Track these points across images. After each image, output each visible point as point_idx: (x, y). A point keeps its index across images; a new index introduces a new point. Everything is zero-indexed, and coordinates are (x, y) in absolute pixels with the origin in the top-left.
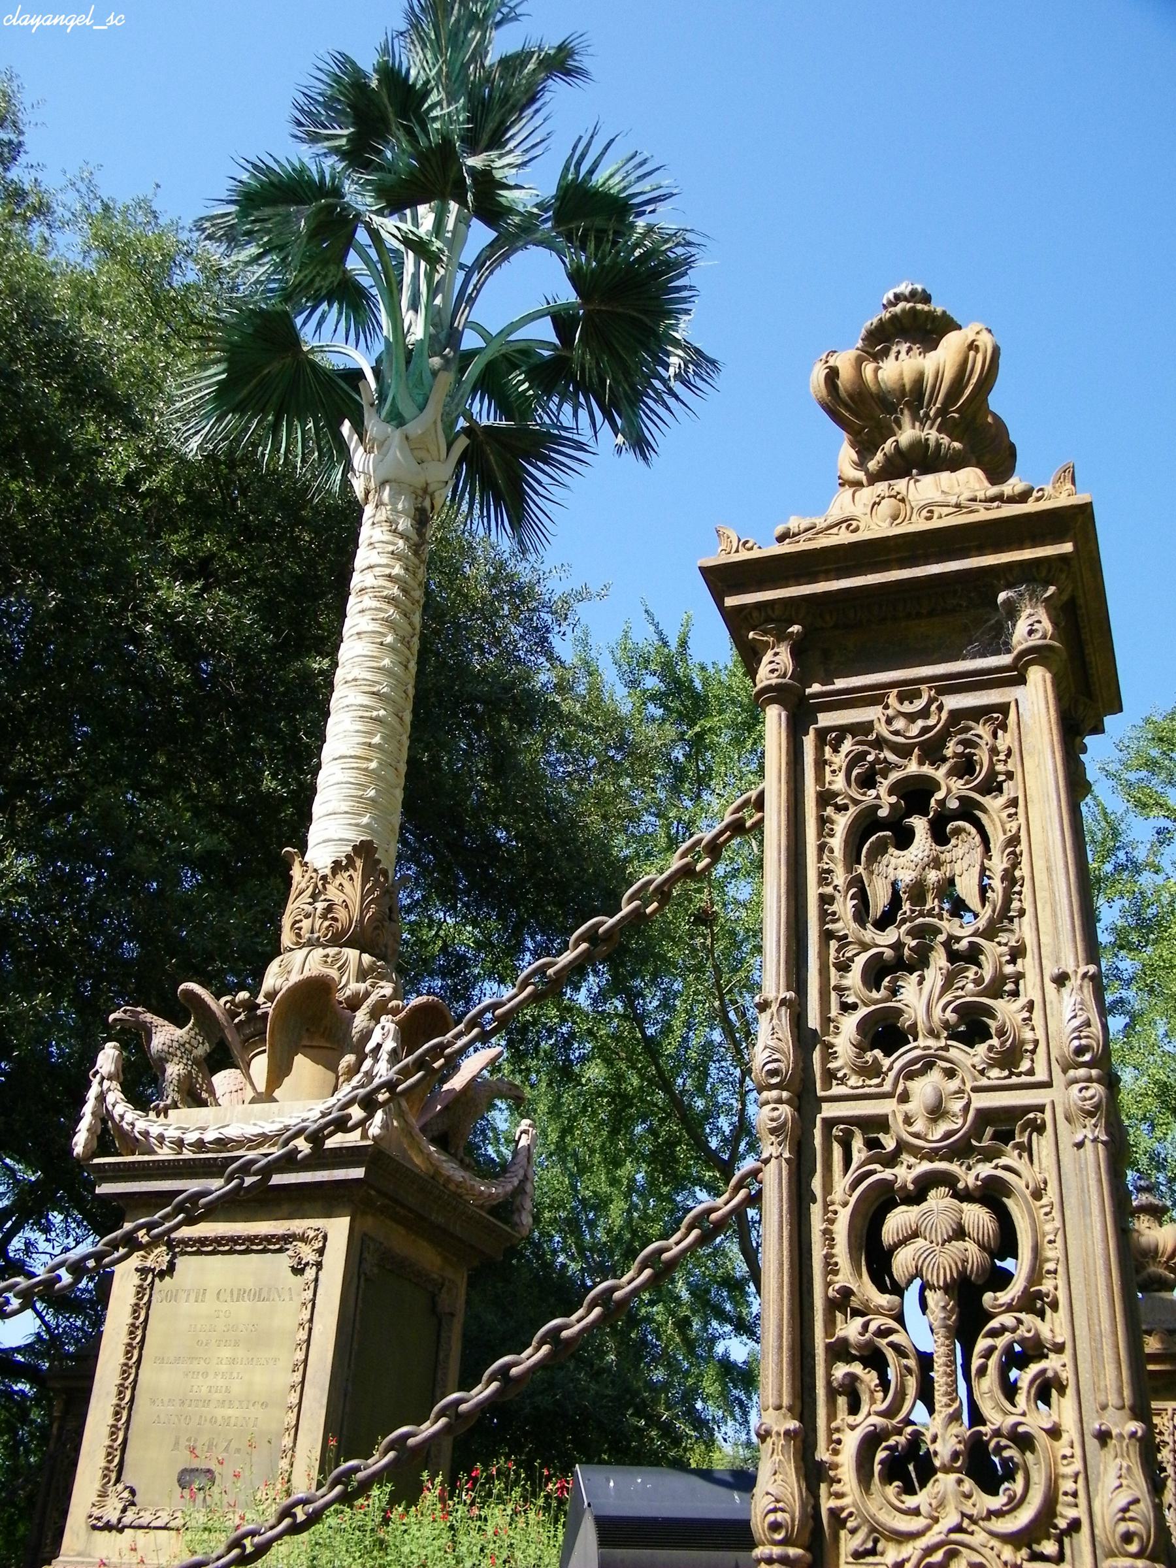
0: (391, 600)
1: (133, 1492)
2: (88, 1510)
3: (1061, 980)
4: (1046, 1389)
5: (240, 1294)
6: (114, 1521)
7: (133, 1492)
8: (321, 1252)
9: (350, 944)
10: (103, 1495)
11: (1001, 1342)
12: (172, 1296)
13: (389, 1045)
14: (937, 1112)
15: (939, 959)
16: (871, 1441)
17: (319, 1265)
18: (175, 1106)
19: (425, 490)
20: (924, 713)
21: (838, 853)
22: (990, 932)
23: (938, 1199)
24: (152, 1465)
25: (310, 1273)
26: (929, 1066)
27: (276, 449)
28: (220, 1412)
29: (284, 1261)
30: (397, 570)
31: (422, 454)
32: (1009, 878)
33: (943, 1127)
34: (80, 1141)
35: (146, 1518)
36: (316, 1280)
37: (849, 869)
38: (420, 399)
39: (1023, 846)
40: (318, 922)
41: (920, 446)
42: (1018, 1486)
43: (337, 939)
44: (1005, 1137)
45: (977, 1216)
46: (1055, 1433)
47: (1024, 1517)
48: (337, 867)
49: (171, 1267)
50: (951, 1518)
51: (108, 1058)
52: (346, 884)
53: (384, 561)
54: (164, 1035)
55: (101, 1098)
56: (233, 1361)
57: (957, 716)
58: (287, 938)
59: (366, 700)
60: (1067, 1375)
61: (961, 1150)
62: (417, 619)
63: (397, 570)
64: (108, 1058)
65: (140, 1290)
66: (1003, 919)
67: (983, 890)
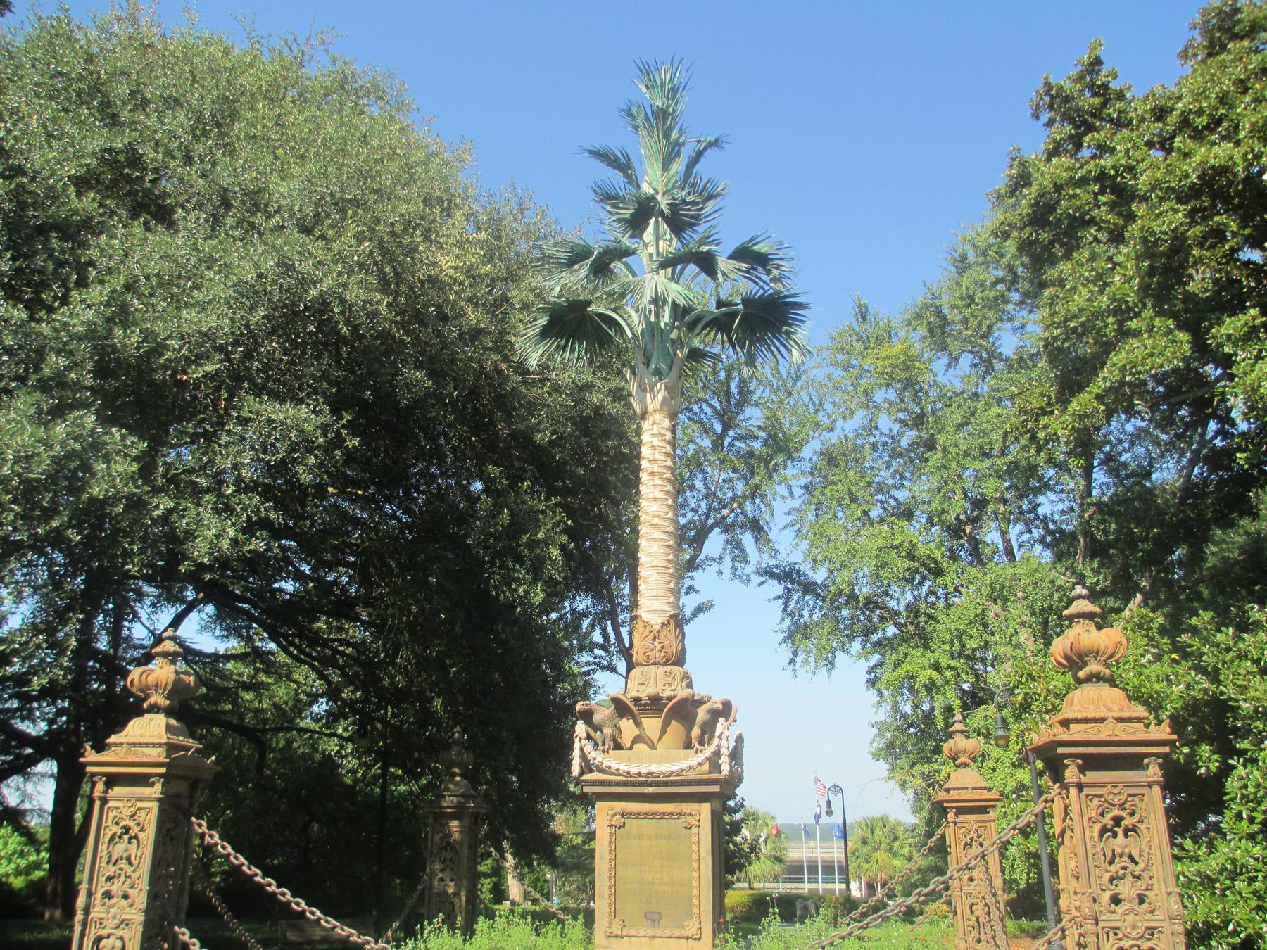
0: (668, 480)
5: (659, 837)
9: (672, 664)
10: (611, 923)
15: (123, 878)
25: (694, 830)
29: (680, 822)
43: (667, 663)
59: (666, 537)
64: (581, 728)
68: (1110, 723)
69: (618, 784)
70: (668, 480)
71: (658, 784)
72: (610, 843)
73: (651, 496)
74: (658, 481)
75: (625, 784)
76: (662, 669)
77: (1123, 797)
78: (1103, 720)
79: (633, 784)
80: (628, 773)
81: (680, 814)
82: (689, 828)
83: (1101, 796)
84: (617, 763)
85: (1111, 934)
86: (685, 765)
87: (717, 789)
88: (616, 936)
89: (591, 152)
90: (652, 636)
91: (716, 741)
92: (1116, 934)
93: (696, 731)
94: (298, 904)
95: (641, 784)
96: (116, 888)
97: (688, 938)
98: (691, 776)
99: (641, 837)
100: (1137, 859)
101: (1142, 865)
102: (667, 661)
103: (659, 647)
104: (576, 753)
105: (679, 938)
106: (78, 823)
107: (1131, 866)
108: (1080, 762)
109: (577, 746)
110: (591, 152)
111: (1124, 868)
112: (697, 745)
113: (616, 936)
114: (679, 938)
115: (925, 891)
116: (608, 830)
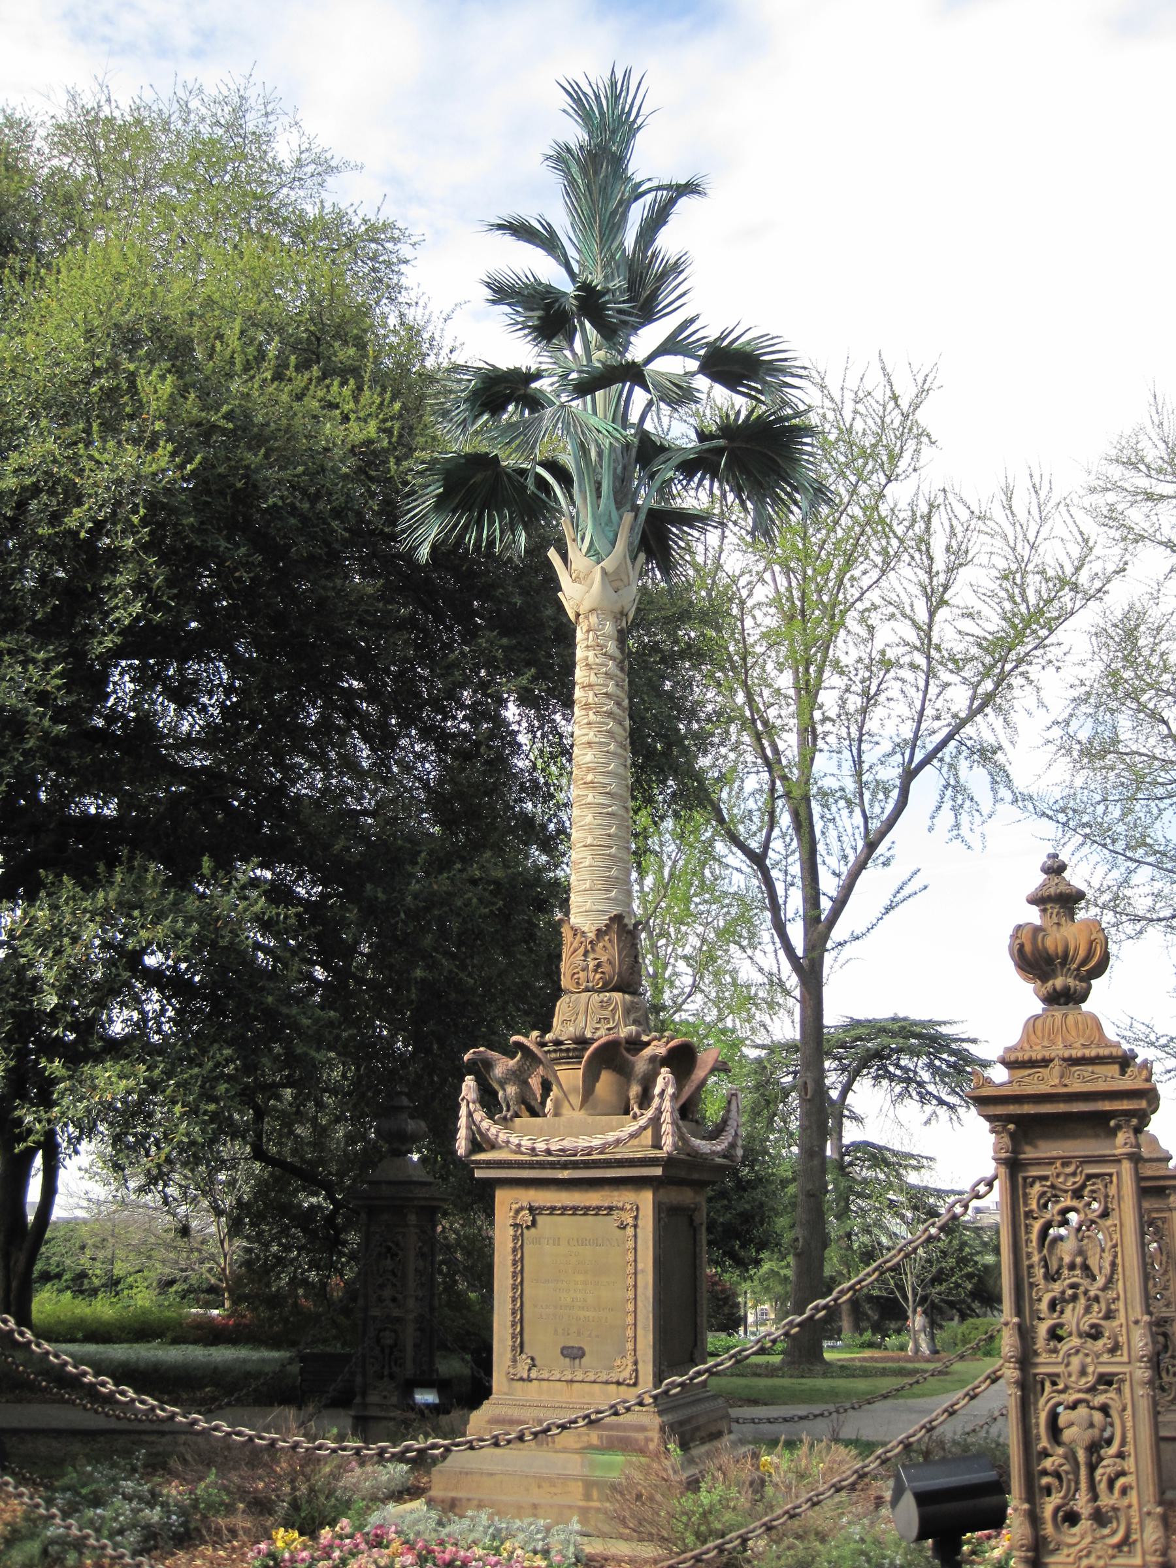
0: (609, 714)
1: (532, 1359)
2: (505, 1369)
3: (1137, 1322)
4: (1124, 1491)
5: (582, 1242)
6: (525, 1376)
7: (532, 1359)
8: (636, 1218)
9: (614, 989)
10: (514, 1361)
11: (1108, 1470)
12: (537, 1241)
13: (670, 1090)
14: (1083, 1373)
15: (1082, 1301)
16: (1057, 1509)
17: (635, 1226)
18: (517, 1115)
19: (622, 613)
20: (1074, 1174)
21: (1034, 1244)
22: (1104, 1289)
23: (1082, 1410)
24: (541, 1341)
25: (630, 1231)
26: (1078, 1352)
27: (480, 534)
28: (582, 1314)
29: (611, 1222)
30: (611, 689)
31: (617, 584)
32: (1113, 1265)
33: (1083, 1380)
34: (461, 1146)
35: (545, 1375)
36: (635, 1236)
37: (1040, 1251)
38: (611, 535)
39: (1119, 1249)
40: (591, 975)
41: (1067, 989)
42: (1115, 1525)
43: (606, 988)
44: (1110, 1383)
45: (1098, 1417)
46: (1130, 1506)
47: (1116, 1539)
48: (600, 933)
49: (534, 1223)
50: (1089, 1539)
51: (469, 1086)
52: (608, 945)
53: (600, 681)
54: (503, 1065)
55: (470, 1115)
56: (585, 1283)
57: (1089, 1177)
58: (565, 982)
59: (600, 799)
60: (1134, 1484)
61: (1092, 1390)
62: (627, 723)
63: (611, 689)
64: (469, 1086)
65: (515, 1238)
66: (1110, 1281)
67: (1100, 1268)
68: (1056, 1068)
69: (520, 1165)
70: (609, 714)
71: (575, 1165)
72: (514, 1250)
73: (585, 739)
74: (592, 717)
75: (531, 1165)
76: (596, 998)
77: (1079, 1179)
78: (1045, 1062)
79: (541, 1165)
80: (533, 1149)
81: (611, 1208)
82: (623, 1227)
83: (1046, 1178)
84: (519, 1139)
85: (1047, 1384)
86: (611, 1137)
87: (658, 1171)
88: (522, 1379)
89: (500, 227)
90: (582, 950)
91: (656, 1101)
92: (1054, 1383)
93: (635, 1090)
94: (22, 1334)
95: (553, 1166)
96: (1072, 1317)
97: (618, 1383)
98: (621, 1153)
99: (556, 1241)
100: (1096, 1271)
101: (1101, 1281)
102: (605, 985)
103: (592, 965)
104: (463, 1122)
105: (607, 1383)
106: (31, 1218)
107: (1085, 1282)
108: (1011, 1127)
109: (463, 1112)
110: (500, 227)
111: (1074, 1286)
112: (636, 1109)
113: (522, 1379)
114: (607, 1383)
115: (799, 1319)
116: (511, 1231)
